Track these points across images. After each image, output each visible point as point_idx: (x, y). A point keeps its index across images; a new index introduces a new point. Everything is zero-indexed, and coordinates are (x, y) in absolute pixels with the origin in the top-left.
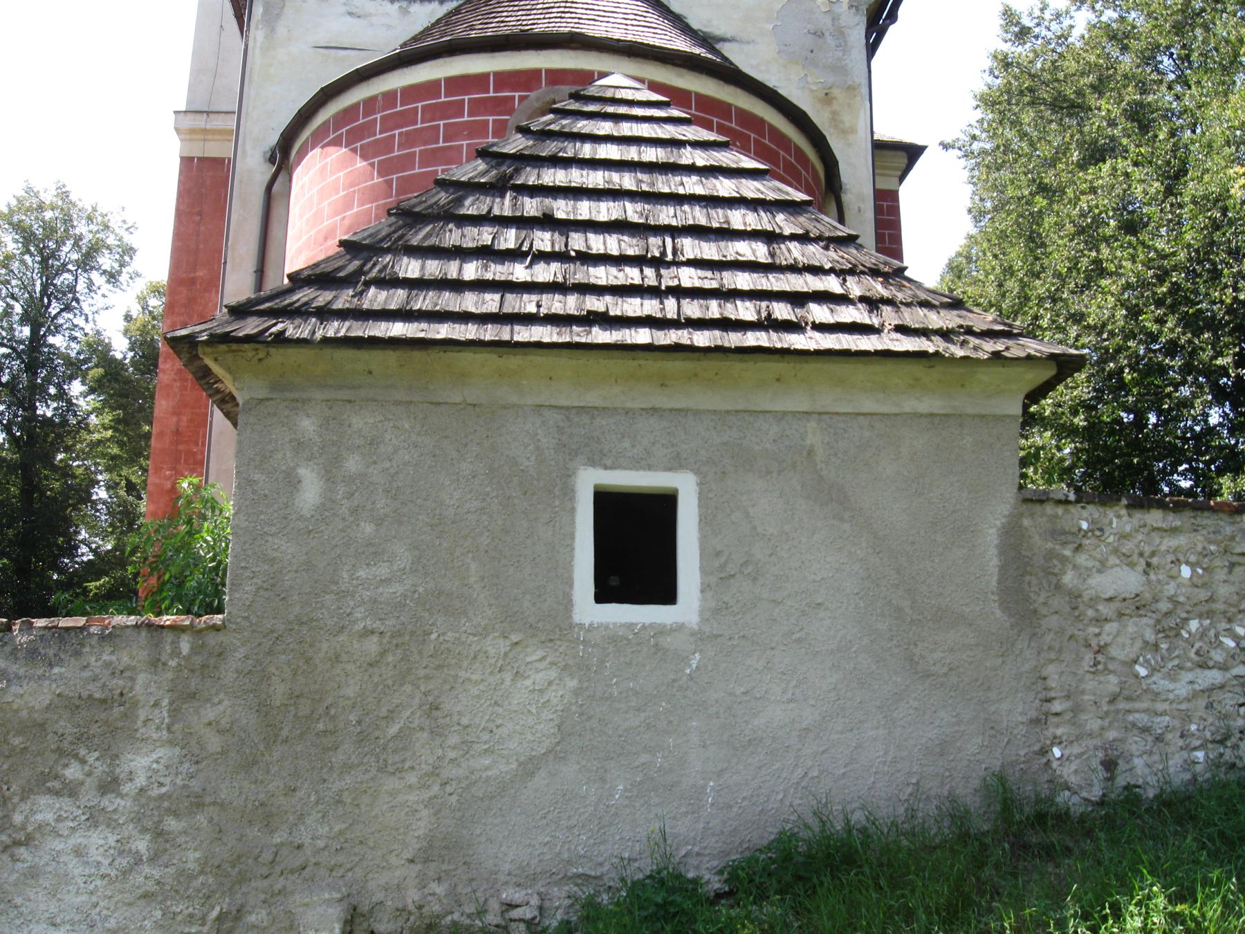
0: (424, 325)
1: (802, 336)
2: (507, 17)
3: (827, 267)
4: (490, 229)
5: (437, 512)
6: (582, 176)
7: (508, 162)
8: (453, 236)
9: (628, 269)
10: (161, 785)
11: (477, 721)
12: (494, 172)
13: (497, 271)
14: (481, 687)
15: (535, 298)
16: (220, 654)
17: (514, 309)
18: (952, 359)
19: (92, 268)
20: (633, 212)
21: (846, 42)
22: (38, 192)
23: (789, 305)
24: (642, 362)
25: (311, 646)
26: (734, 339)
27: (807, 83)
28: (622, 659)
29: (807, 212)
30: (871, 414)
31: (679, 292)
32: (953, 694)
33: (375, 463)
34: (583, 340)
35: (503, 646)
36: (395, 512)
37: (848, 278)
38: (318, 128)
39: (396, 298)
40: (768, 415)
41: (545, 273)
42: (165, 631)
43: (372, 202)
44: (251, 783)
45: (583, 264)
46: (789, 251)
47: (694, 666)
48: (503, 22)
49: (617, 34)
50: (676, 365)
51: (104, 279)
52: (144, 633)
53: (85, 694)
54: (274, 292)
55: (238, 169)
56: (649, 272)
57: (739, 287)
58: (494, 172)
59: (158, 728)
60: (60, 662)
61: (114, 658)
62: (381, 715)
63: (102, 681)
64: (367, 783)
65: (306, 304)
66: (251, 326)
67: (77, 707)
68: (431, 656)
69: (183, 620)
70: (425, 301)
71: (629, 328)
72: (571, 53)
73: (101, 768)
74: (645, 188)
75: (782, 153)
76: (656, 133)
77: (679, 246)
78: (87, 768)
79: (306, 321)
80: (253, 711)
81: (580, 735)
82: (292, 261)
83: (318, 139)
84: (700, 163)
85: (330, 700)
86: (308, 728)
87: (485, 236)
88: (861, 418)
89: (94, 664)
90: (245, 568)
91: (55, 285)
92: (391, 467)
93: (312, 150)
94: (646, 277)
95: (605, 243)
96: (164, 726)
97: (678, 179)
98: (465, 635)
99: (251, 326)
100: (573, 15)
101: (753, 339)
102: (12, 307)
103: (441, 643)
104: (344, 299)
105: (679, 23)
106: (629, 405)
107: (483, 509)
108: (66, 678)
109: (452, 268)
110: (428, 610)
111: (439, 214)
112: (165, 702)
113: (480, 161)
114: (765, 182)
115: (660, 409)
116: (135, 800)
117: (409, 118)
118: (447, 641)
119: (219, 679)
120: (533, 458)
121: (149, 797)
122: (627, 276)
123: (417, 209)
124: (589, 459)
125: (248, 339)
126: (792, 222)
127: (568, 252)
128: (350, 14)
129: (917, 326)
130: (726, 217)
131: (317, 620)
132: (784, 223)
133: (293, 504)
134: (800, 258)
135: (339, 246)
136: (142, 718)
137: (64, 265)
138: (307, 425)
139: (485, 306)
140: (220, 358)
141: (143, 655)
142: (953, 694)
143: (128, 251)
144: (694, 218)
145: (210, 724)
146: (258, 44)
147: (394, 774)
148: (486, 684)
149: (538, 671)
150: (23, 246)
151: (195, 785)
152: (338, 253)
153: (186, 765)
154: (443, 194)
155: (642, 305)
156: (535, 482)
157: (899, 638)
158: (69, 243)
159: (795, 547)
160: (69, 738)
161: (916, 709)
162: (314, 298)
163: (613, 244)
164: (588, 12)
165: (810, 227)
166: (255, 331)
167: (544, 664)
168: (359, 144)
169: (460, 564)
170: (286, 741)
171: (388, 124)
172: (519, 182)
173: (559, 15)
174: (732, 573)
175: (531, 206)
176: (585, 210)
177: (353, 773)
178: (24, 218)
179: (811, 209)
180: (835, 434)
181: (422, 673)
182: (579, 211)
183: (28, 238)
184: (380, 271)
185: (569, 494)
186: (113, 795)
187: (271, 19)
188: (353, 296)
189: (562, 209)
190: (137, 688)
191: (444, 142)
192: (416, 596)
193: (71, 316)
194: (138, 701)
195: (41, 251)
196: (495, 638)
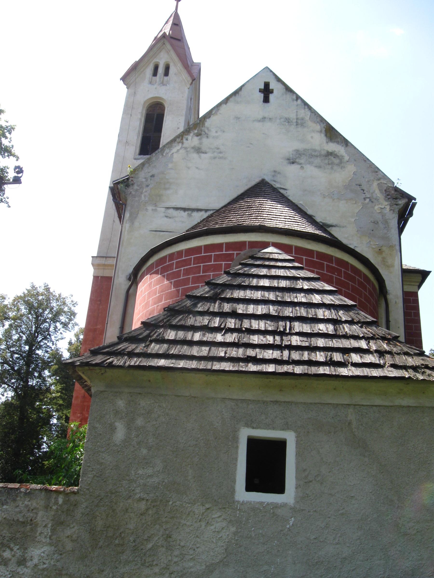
0: (174, 361)
1: (346, 369)
2: (232, 218)
3: (361, 335)
4: (208, 318)
5: (176, 445)
6: (251, 293)
7: (219, 287)
8: (191, 321)
9: (268, 337)
10: (44, 563)
11: (188, 544)
12: (212, 292)
13: (209, 337)
14: (191, 528)
15: (224, 349)
16: (75, 505)
17: (214, 354)
18: (417, 380)
19: (57, 321)
20: (272, 310)
21: (388, 226)
22: (37, 288)
23: (341, 354)
24: (271, 380)
25: (116, 504)
26: (314, 370)
27: (371, 245)
28: (257, 519)
29: (353, 310)
30: (379, 406)
31: (290, 348)
32: (419, 544)
33: (149, 422)
34: (244, 370)
35: (202, 509)
36: (157, 444)
37: (371, 341)
38: (149, 266)
39: (162, 348)
40: (329, 405)
41: (230, 338)
42: (52, 493)
43: (170, 299)
44: (83, 566)
45: (248, 334)
46: (344, 328)
47: (291, 524)
48: (230, 221)
49: (281, 226)
50: (287, 381)
51: (62, 326)
52: (43, 493)
53: (16, 519)
54: (111, 344)
55: (115, 283)
56: (278, 338)
57: (318, 345)
58: (212, 292)
59: (45, 537)
60: (7, 503)
61: (30, 503)
62: (145, 538)
63: (23, 513)
64: (136, 570)
65: (124, 350)
66: (98, 359)
67: (12, 524)
68: (169, 512)
69: (61, 488)
70: (174, 351)
71: (265, 364)
72: (260, 234)
73: (19, 553)
74: (279, 299)
75: (357, 277)
76: (287, 274)
77: (293, 326)
78: (13, 553)
79: (122, 358)
80: (88, 532)
81: (235, 554)
82: (135, 324)
83: (149, 271)
84: (306, 287)
85: (122, 530)
86: (111, 542)
87: (205, 320)
88: (374, 408)
89: (21, 505)
90: (89, 466)
91: (41, 328)
92: (156, 424)
93: (146, 276)
94: (276, 340)
95: (259, 325)
96: (48, 536)
97: (295, 295)
98: (185, 503)
99: (98, 359)
100: (262, 217)
101: (322, 370)
102: (22, 337)
103: (174, 506)
104: (140, 348)
105: (310, 219)
106: (265, 399)
107: (196, 445)
108: (8, 511)
109: (189, 335)
110: (169, 490)
111: (186, 310)
112: (50, 525)
113: (206, 287)
114: (335, 296)
115: (279, 401)
116: (32, 570)
117: (187, 262)
118: (177, 506)
119: (74, 516)
120: (220, 422)
121: (39, 569)
122: (267, 340)
123: (176, 308)
124: (246, 424)
125: (97, 365)
126: (346, 315)
127: (241, 328)
128: (166, 217)
129: (401, 364)
130: (315, 312)
131: (119, 492)
132: (343, 315)
133: (112, 439)
134: (348, 332)
135: (141, 324)
136: (39, 532)
137: (45, 319)
138: (121, 403)
139: (202, 353)
140: (85, 372)
141: (42, 503)
142: (419, 544)
143: (73, 314)
144: (300, 313)
145: (68, 537)
146: (127, 229)
147: (148, 567)
148: (193, 527)
149: (217, 522)
150: (29, 311)
151: (59, 565)
152: (140, 327)
153: (56, 555)
154: (189, 301)
155: (273, 353)
156: (221, 433)
157: (392, 515)
158: (48, 310)
159: (342, 468)
160: (7, 539)
161: (400, 551)
162: (127, 347)
163: (262, 325)
164: (268, 216)
165: (354, 317)
166: (100, 361)
167: (220, 519)
168: (166, 274)
169: (184, 470)
170: (101, 547)
171: (179, 265)
172: (223, 296)
173: (255, 217)
174: (311, 480)
175: (227, 307)
176: (251, 309)
177: (129, 565)
178: (30, 299)
179: (356, 309)
180: (362, 415)
181: (164, 520)
182: (249, 310)
183: (30, 307)
184: (157, 336)
185: (236, 439)
186: (23, 567)
187: (132, 219)
188: (144, 347)
189: (241, 309)
190: (38, 518)
191: (202, 273)
192: (164, 483)
193: (46, 342)
194: (38, 524)
195: (36, 313)
196: (198, 506)
